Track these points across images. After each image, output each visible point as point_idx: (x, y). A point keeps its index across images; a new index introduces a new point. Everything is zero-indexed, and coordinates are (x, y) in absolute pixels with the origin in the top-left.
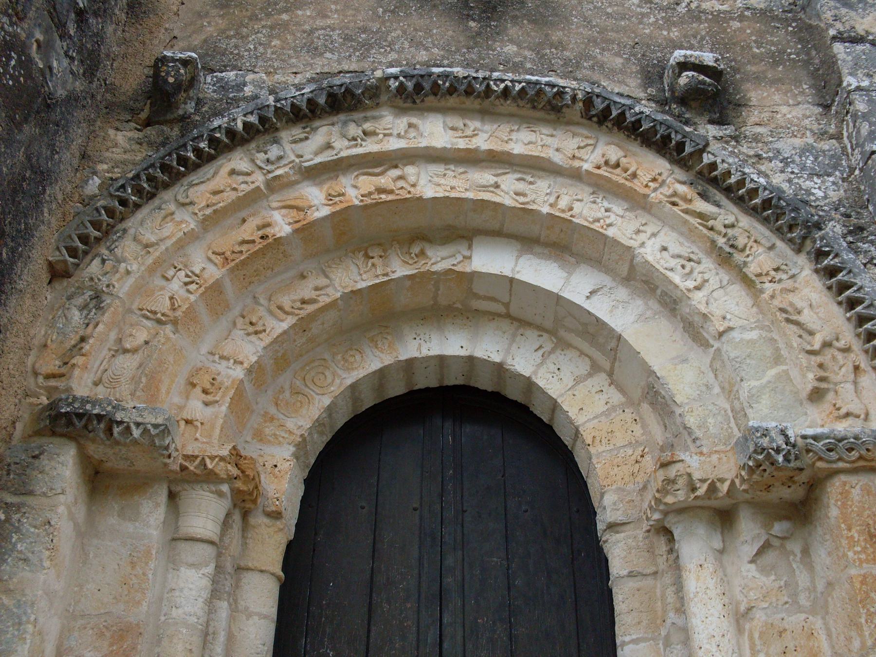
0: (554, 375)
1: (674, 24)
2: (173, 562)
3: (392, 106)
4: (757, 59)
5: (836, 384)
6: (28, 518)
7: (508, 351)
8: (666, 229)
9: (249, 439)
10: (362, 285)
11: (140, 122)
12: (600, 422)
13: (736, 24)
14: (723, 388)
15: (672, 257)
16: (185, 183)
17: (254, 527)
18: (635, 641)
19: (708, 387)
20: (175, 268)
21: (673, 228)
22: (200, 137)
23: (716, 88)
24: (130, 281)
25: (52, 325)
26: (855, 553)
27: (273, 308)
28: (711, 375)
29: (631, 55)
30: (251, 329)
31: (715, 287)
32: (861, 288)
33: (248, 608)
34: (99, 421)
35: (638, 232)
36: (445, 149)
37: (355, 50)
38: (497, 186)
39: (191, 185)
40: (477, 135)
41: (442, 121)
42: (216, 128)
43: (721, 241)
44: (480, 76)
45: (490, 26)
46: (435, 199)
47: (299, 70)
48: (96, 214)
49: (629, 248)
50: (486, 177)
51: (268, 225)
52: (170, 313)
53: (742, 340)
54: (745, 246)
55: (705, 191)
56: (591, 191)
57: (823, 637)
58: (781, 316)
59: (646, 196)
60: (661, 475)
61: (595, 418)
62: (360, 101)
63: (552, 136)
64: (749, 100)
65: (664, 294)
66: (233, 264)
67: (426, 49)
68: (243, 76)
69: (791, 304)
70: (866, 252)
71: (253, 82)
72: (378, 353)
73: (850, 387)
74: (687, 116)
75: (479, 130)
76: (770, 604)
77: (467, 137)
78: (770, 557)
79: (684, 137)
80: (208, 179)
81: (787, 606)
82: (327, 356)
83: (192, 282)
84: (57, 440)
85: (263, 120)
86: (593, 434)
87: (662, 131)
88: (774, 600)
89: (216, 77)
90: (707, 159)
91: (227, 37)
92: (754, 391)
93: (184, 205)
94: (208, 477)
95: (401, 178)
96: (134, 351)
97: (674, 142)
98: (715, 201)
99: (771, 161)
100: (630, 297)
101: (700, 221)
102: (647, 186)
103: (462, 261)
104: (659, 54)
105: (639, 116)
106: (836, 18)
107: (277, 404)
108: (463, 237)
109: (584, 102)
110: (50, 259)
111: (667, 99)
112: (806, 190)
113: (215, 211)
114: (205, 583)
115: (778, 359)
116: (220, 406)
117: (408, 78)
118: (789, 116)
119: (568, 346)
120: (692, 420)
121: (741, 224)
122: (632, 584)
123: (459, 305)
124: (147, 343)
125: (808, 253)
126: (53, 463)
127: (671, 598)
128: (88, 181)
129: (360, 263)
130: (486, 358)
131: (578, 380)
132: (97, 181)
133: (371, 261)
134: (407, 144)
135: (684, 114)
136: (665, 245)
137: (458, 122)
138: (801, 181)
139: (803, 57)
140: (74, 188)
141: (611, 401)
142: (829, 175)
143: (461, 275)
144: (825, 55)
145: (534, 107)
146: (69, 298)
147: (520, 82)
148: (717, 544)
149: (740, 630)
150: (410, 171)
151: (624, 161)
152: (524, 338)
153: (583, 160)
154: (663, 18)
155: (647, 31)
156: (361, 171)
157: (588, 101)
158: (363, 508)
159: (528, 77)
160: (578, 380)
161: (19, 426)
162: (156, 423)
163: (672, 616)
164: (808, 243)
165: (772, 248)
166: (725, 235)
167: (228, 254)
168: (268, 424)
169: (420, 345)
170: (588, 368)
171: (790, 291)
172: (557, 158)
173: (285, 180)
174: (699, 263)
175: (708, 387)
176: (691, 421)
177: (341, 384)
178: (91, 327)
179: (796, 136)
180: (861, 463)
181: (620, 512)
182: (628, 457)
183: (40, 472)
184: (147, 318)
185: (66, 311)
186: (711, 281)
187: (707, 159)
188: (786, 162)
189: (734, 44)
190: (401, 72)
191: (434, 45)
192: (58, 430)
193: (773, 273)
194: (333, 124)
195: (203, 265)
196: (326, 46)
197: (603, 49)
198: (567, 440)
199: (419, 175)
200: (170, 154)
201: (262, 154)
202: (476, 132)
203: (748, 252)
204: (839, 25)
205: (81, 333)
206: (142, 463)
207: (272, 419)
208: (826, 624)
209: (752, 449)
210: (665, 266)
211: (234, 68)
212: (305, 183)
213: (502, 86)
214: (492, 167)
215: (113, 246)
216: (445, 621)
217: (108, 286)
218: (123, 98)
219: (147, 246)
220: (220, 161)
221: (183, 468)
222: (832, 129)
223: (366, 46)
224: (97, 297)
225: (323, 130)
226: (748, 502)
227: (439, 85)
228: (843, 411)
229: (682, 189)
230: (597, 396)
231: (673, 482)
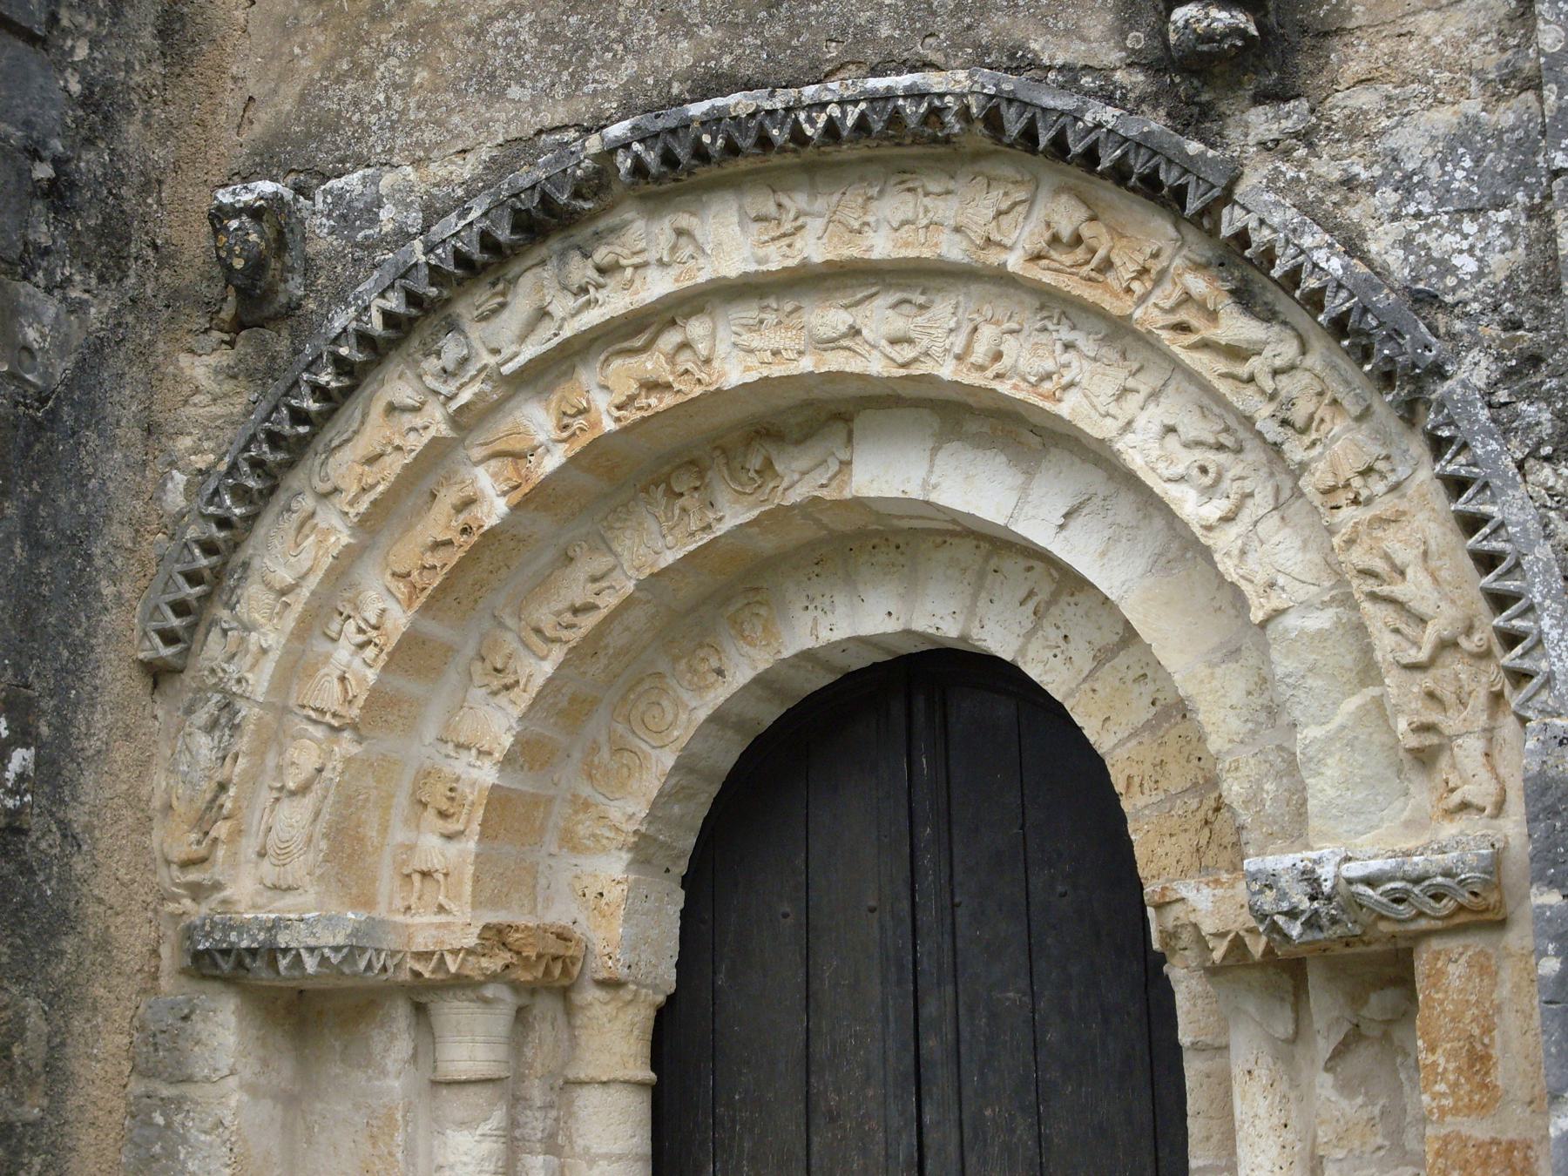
0: (1057, 651)
3: (644, 198)
6: (193, 1120)
9: (554, 849)
10: (669, 558)
11: (226, 327)
12: (1140, 743)
15: (1186, 446)
16: (320, 448)
17: (582, 1008)
20: (341, 614)
24: (269, 666)
30: (496, 684)
31: (1261, 512)
32: (1502, 525)
33: (589, 1149)
37: (564, 65)
38: (855, 332)
40: (802, 227)
41: (735, 207)
42: (340, 334)
44: (779, 106)
47: (468, 144)
50: (830, 317)
51: (468, 503)
53: (1302, 632)
56: (1037, 304)
61: (1130, 736)
63: (948, 192)
67: (689, 35)
68: (375, 181)
69: (1387, 557)
72: (747, 648)
74: (1205, 97)
75: (806, 214)
76: (1351, 1150)
77: (784, 235)
78: (1361, 1059)
79: (1186, 171)
80: (356, 432)
81: (1382, 1153)
85: (412, 298)
86: (1127, 772)
88: (1357, 1143)
89: (330, 191)
93: (325, 496)
95: (685, 345)
96: (304, 789)
98: (1266, 303)
99: (1373, 192)
100: (1141, 514)
103: (840, 471)
105: (1093, 136)
110: (141, 656)
117: (649, 142)
118: (1437, 40)
120: (1236, 788)
128: (165, 484)
129: (660, 512)
130: (932, 631)
132: (180, 478)
134: (677, 280)
135: (1198, 94)
136: (1170, 422)
140: (147, 503)
141: (1160, 696)
142: (1499, 205)
147: (856, 102)
148: (1283, 1027)
150: (697, 329)
151: (1086, 231)
152: (999, 577)
153: (1005, 247)
156: (610, 349)
157: (993, 120)
158: (785, 916)
161: (165, 951)
162: (335, 944)
166: (1272, 397)
168: (581, 816)
169: (815, 619)
171: (1389, 521)
172: (953, 250)
173: (481, 405)
177: (689, 721)
179: (1442, 102)
180: (1462, 918)
182: (1190, 816)
183: (197, 1043)
184: (315, 722)
185: (188, 740)
186: (1258, 498)
188: (1407, 187)
190: (634, 128)
193: (1357, 482)
194: (543, 263)
195: (381, 606)
199: (713, 335)
201: (433, 360)
202: (799, 222)
207: (586, 805)
210: (1167, 474)
211: (362, 162)
212: (521, 397)
213: (822, 120)
215: (234, 599)
216: (927, 1119)
217: (239, 681)
219: (283, 593)
225: (527, 281)
228: (1456, 798)
229: (1197, 284)
230: (1136, 688)
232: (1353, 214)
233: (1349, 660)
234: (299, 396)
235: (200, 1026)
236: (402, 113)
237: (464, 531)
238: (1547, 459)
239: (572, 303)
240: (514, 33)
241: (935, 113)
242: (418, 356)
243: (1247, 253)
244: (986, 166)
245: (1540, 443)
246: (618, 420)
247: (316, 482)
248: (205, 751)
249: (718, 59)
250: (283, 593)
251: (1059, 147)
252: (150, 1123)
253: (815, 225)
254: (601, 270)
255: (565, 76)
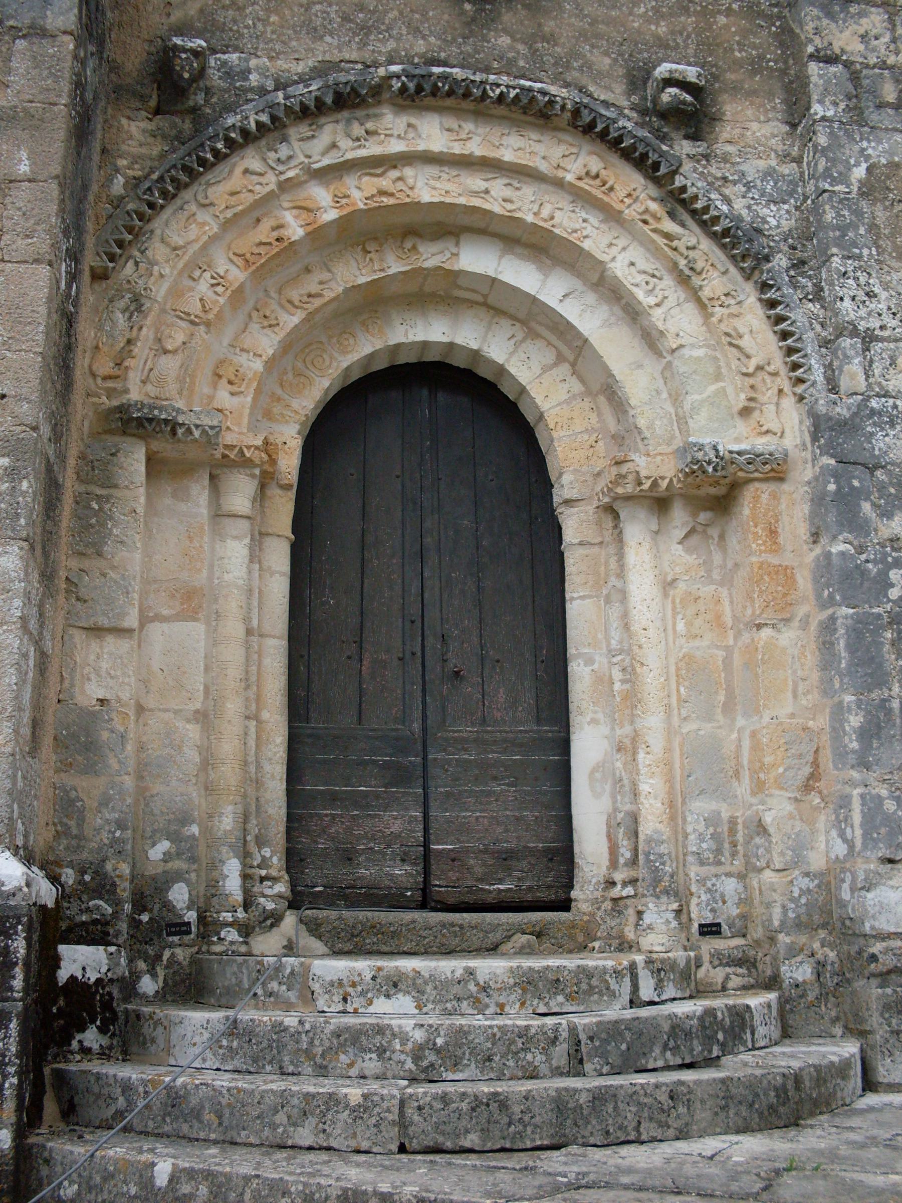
1: (663, 17)
2: (218, 534)
3: (394, 105)
4: (738, 64)
5: (762, 404)
7: (484, 339)
8: (635, 243)
10: (362, 280)
13: (722, 20)
14: (670, 395)
15: (639, 272)
18: (582, 598)
19: (658, 392)
21: (642, 244)
22: (214, 138)
23: (695, 107)
24: (165, 286)
25: (100, 328)
26: (758, 545)
27: (284, 302)
28: (661, 381)
29: (619, 55)
30: (266, 323)
32: (794, 322)
34: (166, 426)
35: (611, 245)
36: (441, 152)
37: (355, 34)
38: (487, 192)
39: (209, 184)
43: (682, 263)
45: (484, 10)
46: (431, 204)
47: (301, 57)
48: (128, 219)
49: (602, 262)
50: (476, 182)
51: (280, 227)
52: (201, 315)
54: (703, 270)
55: (673, 210)
57: (727, 603)
58: (725, 340)
59: (620, 212)
60: (614, 471)
62: (364, 101)
63: (539, 141)
64: (724, 114)
65: (628, 304)
66: (254, 267)
67: (424, 38)
68: (247, 61)
69: (735, 329)
70: (804, 287)
71: (257, 68)
73: (772, 408)
74: (665, 130)
78: (695, 540)
79: (661, 156)
82: (324, 339)
83: (218, 284)
84: (129, 439)
85: (274, 118)
87: (641, 149)
89: (219, 59)
90: (679, 181)
91: (223, 7)
92: (695, 405)
93: (204, 206)
94: (244, 463)
95: (400, 179)
96: (175, 352)
97: (650, 161)
101: (666, 241)
102: (622, 201)
104: (645, 55)
105: (621, 131)
106: (817, 31)
107: (281, 385)
108: (450, 233)
109: (572, 112)
111: (647, 109)
112: (762, 218)
113: (235, 215)
114: (246, 552)
115: (718, 377)
116: (245, 397)
118: (758, 134)
119: (538, 336)
120: (642, 421)
121: (701, 247)
122: (582, 551)
123: (442, 293)
124: (184, 343)
125: (756, 282)
126: (129, 460)
127: (613, 564)
129: (359, 258)
131: (546, 369)
132: (120, 180)
133: (369, 256)
137: (452, 123)
138: (758, 208)
139: (780, 65)
142: (784, 203)
143: (449, 272)
144: (800, 70)
145: (525, 113)
146: (111, 301)
147: (514, 88)
148: (655, 527)
149: (665, 595)
151: (603, 173)
154: (653, 7)
155: (636, 25)
157: (576, 113)
159: (522, 82)
160: (546, 369)
163: (613, 581)
164: (757, 272)
165: (725, 273)
166: (686, 258)
167: (248, 256)
170: (554, 358)
172: (543, 167)
173: (295, 181)
174: (660, 279)
175: (658, 392)
176: (642, 422)
177: (338, 366)
178: (135, 329)
180: (772, 474)
181: (575, 491)
184: (181, 319)
186: (670, 299)
187: (679, 181)
188: (748, 186)
189: (717, 45)
190: (403, 70)
191: (431, 31)
192: (128, 431)
193: (723, 298)
194: (337, 122)
196: (325, 27)
197: (593, 46)
198: (530, 419)
199: (416, 177)
200: (189, 155)
203: (704, 276)
204: (818, 41)
205: (128, 336)
206: (193, 453)
207: (279, 399)
208: (730, 594)
209: (689, 460)
210: (633, 281)
211: (236, 49)
212: (313, 182)
213: (498, 91)
214: (482, 171)
216: (426, 574)
217: (145, 289)
218: (128, 80)
219: (175, 249)
220: (234, 159)
221: (225, 456)
222: (795, 151)
223: (365, 29)
224: (137, 300)
225: (328, 128)
226: (681, 495)
227: (438, 88)
228: (764, 428)
229: (654, 206)
231: (624, 477)
232: (727, 192)
233: (711, 370)
234: (204, 151)
235: (123, 459)
236: (262, 33)
237: (277, 240)
238: (810, 300)
239: (350, 143)
240: (328, 13)
241: (551, 103)
242: (264, 150)
243: (684, 196)
244: (561, 135)
245: (808, 294)
246: (366, 204)
247: (199, 198)
248: (121, 321)
249: (439, 53)
250: (175, 249)
251: (605, 132)
252: (89, 507)
253: (477, 139)
254: (367, 132)
255: (357, 39)
